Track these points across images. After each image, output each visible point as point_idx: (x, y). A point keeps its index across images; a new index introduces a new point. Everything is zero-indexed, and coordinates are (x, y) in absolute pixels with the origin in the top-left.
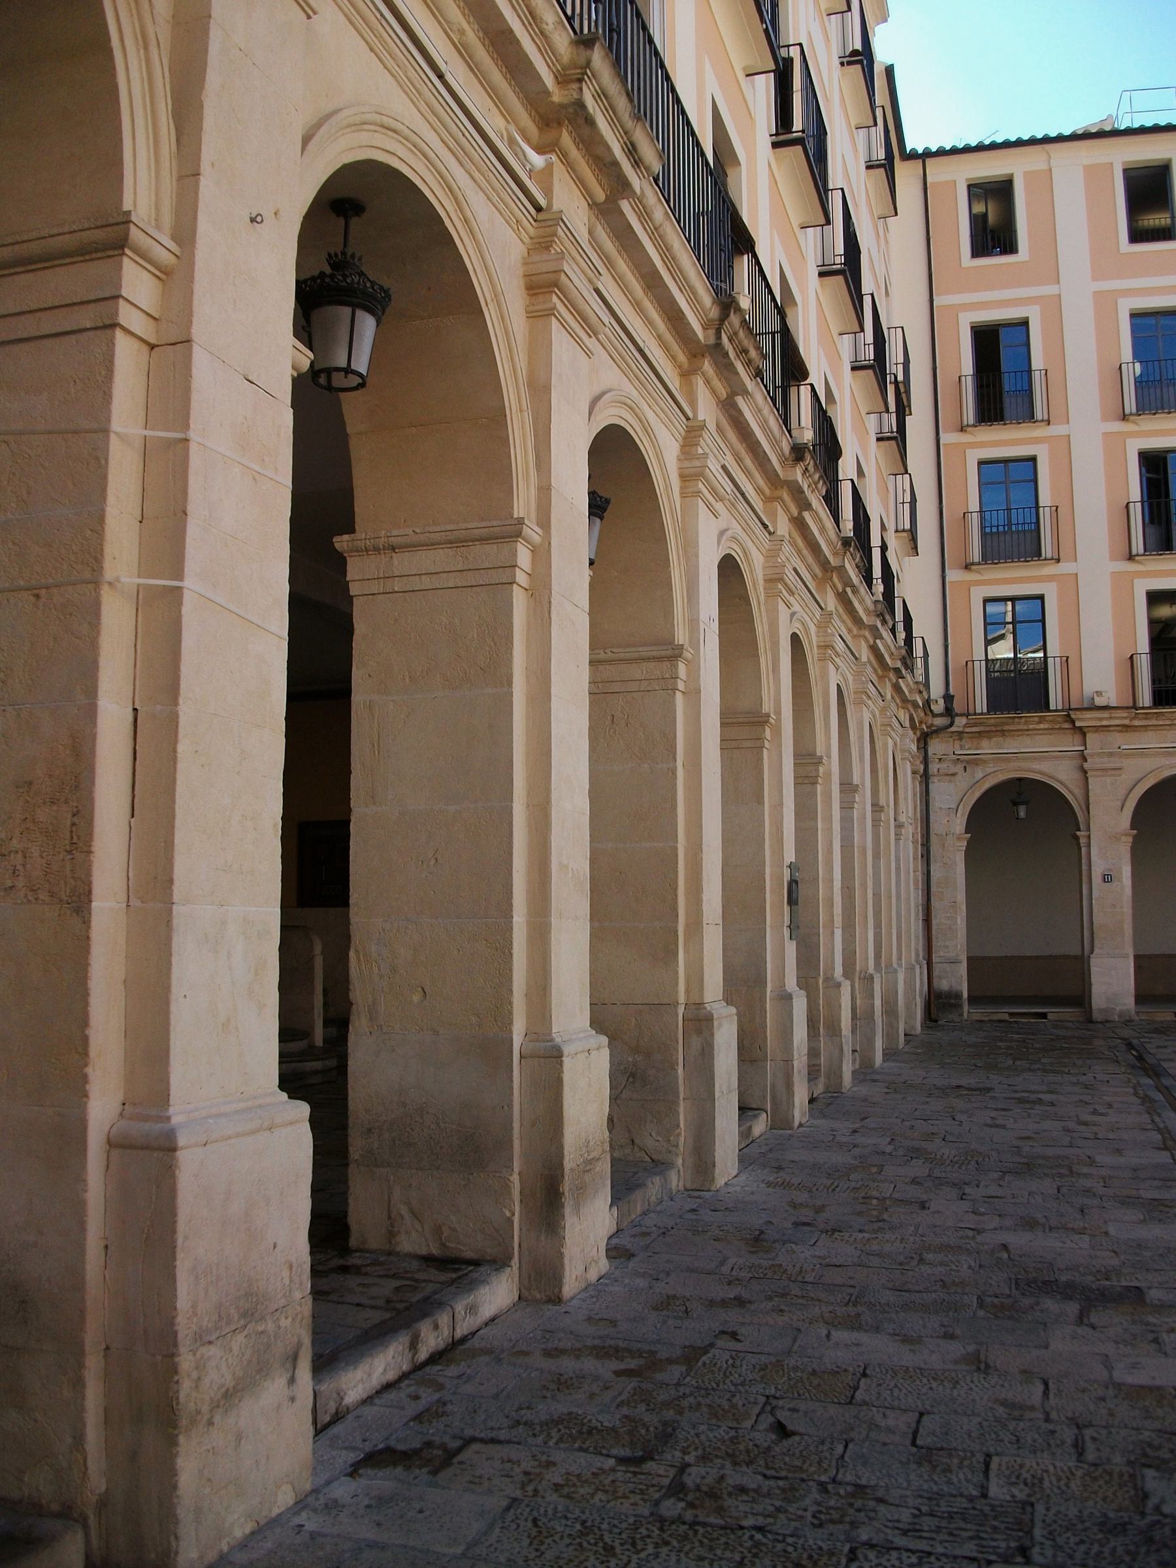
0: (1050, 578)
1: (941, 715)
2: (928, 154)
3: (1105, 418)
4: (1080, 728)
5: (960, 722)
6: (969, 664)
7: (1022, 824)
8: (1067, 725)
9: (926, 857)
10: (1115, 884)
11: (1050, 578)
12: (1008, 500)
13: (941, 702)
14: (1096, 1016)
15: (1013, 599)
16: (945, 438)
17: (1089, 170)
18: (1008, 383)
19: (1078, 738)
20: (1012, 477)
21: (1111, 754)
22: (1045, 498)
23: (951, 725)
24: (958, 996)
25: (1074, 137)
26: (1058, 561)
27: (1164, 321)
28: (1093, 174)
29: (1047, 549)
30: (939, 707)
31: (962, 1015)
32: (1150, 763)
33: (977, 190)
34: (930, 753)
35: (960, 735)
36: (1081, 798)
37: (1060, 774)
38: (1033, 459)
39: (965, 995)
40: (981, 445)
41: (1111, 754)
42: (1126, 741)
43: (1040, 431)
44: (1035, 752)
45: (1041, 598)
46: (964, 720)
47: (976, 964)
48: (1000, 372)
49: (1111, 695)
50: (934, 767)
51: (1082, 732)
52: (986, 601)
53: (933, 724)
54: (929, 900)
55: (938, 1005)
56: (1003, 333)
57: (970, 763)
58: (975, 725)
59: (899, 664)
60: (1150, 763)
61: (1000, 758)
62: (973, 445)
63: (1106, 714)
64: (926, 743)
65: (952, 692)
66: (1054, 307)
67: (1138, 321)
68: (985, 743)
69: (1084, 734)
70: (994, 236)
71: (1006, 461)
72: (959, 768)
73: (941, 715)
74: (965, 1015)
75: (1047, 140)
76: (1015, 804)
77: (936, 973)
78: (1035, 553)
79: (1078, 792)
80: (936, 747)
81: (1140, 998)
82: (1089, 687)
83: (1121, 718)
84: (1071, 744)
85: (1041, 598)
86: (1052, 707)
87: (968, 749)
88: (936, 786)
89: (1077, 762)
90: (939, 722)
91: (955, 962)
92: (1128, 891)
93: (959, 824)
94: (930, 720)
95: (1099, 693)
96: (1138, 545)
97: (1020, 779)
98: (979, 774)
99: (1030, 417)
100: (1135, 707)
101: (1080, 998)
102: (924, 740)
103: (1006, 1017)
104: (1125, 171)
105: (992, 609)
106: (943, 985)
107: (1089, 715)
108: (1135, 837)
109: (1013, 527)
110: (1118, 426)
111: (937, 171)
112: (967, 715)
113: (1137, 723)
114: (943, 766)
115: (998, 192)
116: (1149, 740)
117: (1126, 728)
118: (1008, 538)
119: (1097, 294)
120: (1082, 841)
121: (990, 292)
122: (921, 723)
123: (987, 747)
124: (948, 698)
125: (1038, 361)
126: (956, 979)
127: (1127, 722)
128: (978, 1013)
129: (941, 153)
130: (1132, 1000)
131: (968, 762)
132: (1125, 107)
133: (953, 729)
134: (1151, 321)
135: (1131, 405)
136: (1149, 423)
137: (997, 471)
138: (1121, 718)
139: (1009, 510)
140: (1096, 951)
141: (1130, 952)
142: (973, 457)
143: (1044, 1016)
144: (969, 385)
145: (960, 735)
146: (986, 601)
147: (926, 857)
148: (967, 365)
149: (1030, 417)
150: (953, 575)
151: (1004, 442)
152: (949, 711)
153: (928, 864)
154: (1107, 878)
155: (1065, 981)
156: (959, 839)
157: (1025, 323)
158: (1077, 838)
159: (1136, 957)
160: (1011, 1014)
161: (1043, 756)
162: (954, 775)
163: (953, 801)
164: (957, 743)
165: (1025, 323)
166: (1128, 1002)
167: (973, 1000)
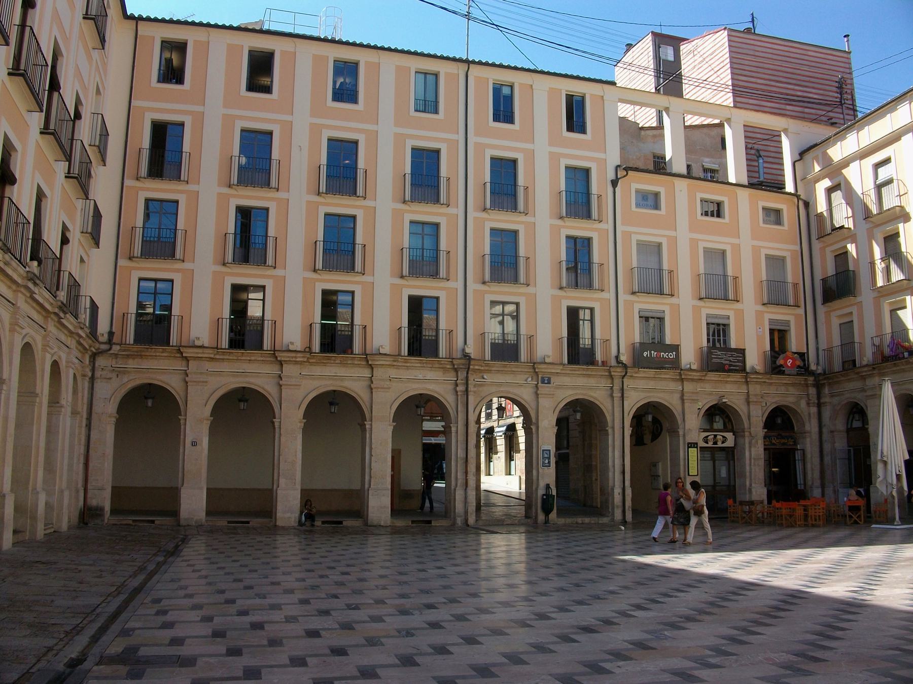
0: (178, 271)
1: (105, 343)
2: (140, 18)
3: (308, 193)
4: (186, 357)
5: (116, 348)
6: (829, 350)
7: (150, 409)
8: (178, 355)
9: (89, 426)
10: (198, 447)
11: (667, 304)
12: (160, 224)
13: (106, 336)
14: (182, 522)
15: (156, 280)
16: (127, 182)
17: (399, 69)
18: (168, 156)
19: (184, 363)
20: (161, 212)
21: (201, 373)
22: (181, 225)
23: (110, 349)
24: (102, 509)
25: (239, 29)
26: (275, 268)
27: (260, 137)
28: (232, 50)
29: (178, 254)
30: (105, 338)
31: (103, 521)
32: (316, 383)
33: (167, 45)
34: (97, 365)
35: (116, 356)
36: (534, 407)
37: (173, 383)
38: (177, 202)
39: (107, 508)
40: (148, 189)
41: (201, 373)
42: (393, 373)
43: (360, 202)
44: (160, 369)
45: (172, 281)
46: (118, 347)
47: (117, 492)
48: (164, 150)
49: (205, 340)
50: (98, 374)
51: (187, 359)
52: (140, 279)
53: (97, 349)
54: (88, 451)
55: (88, 515)
56: (169, 126)
57: (120, 372)
58: (124, 351)
59: (56, 310)
60: (316, 383)
61: (139, 370)
62: (564, 227)
63: (200, 350)
64: (94, 359)
65: (114, 330)
66: (199, 118)
67: (244, 134)
68: (130, 361)
69: (282, 365)
70: (346, 93)
71: (339, 216)
72: (114, 375)
73: (105, 343)
74: (106, 521)
75: (208, 25)
76: (146, 398)
77: (89, 495)
78: (435, 275)
79: (182, 394)
80: (101, 362)
81: (209, 513)
82: (193, 334)
83: (209, 353)
84: (180, 365)
85: (172, 281)
86: (265, 348)
87: (120, 364)
88: (98, 385)
89: (368, 383)
90: (104, 347)
91: (102, 489)
92: (206, 452)
93: (112, 408)
94: (97, 345)
95: (198, 339)
96: (229, 258)
97: (150, 384)
98: (125, 380)
99: (178, 178)
100: (399, 355)
101: (175, 513)
102: (94, 356)
103: (131, 522)
104: (250, 51)
105: (143, 284)
106: (93, 502)
107: (191, 350)
108: (394, 427)
109: (160, 237)
110: (560, 222)
111: (474, 71)
112: (120, 344)
113: (218, 357)
114: (104, 373)
115: (181, 47)
116: (225, 367)
117: (212, 359)
118: (156, 244)
119: (396, 135)
120: (277, 425)
121: (165, 104)
122: (90, 346)
123: (132, 364)
124: (111, 334)
125: (186, 147)
126: (104, 499)
127: (212, 356)
128: (115, 520)
129: (148, 19)
130: (204, 514)
131: (119, 372)
132: (267, 18)
133: (111, 352)
134: (253, 135)
135: (235, 180)
136: (416, 207)
137: (419, 229)
138: (209, 353)
139: (423, 249)
140: (185, 485)
141: (299, 487)
142: (142, 196)
143: (153, 522)
144: (145, 155)
145: (116, 356)
146: (140, 279)
147: (89, 426)
148: (146, 143)
149: (178, 178)
150: (122, 262)
151: (161, 189)
152: (110, 342)
153: (89, 430)
154: (194, 444)
155: (166, 502)
156: (110, 417)
157: (182, 125)
158: (273, 423)
159: (208, 489)
160: (134, 521)
161: (164, 371)
162: (110, 379)
163: (109, 395)
164: (114, 361)
165: (182, 125)
166: (202, 515)
167: (114, 512)
